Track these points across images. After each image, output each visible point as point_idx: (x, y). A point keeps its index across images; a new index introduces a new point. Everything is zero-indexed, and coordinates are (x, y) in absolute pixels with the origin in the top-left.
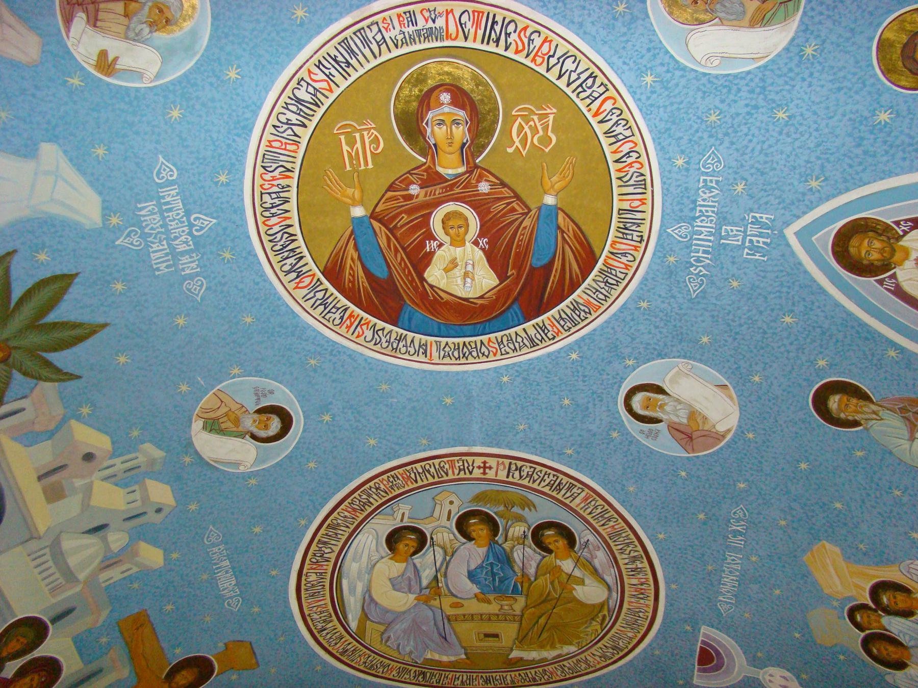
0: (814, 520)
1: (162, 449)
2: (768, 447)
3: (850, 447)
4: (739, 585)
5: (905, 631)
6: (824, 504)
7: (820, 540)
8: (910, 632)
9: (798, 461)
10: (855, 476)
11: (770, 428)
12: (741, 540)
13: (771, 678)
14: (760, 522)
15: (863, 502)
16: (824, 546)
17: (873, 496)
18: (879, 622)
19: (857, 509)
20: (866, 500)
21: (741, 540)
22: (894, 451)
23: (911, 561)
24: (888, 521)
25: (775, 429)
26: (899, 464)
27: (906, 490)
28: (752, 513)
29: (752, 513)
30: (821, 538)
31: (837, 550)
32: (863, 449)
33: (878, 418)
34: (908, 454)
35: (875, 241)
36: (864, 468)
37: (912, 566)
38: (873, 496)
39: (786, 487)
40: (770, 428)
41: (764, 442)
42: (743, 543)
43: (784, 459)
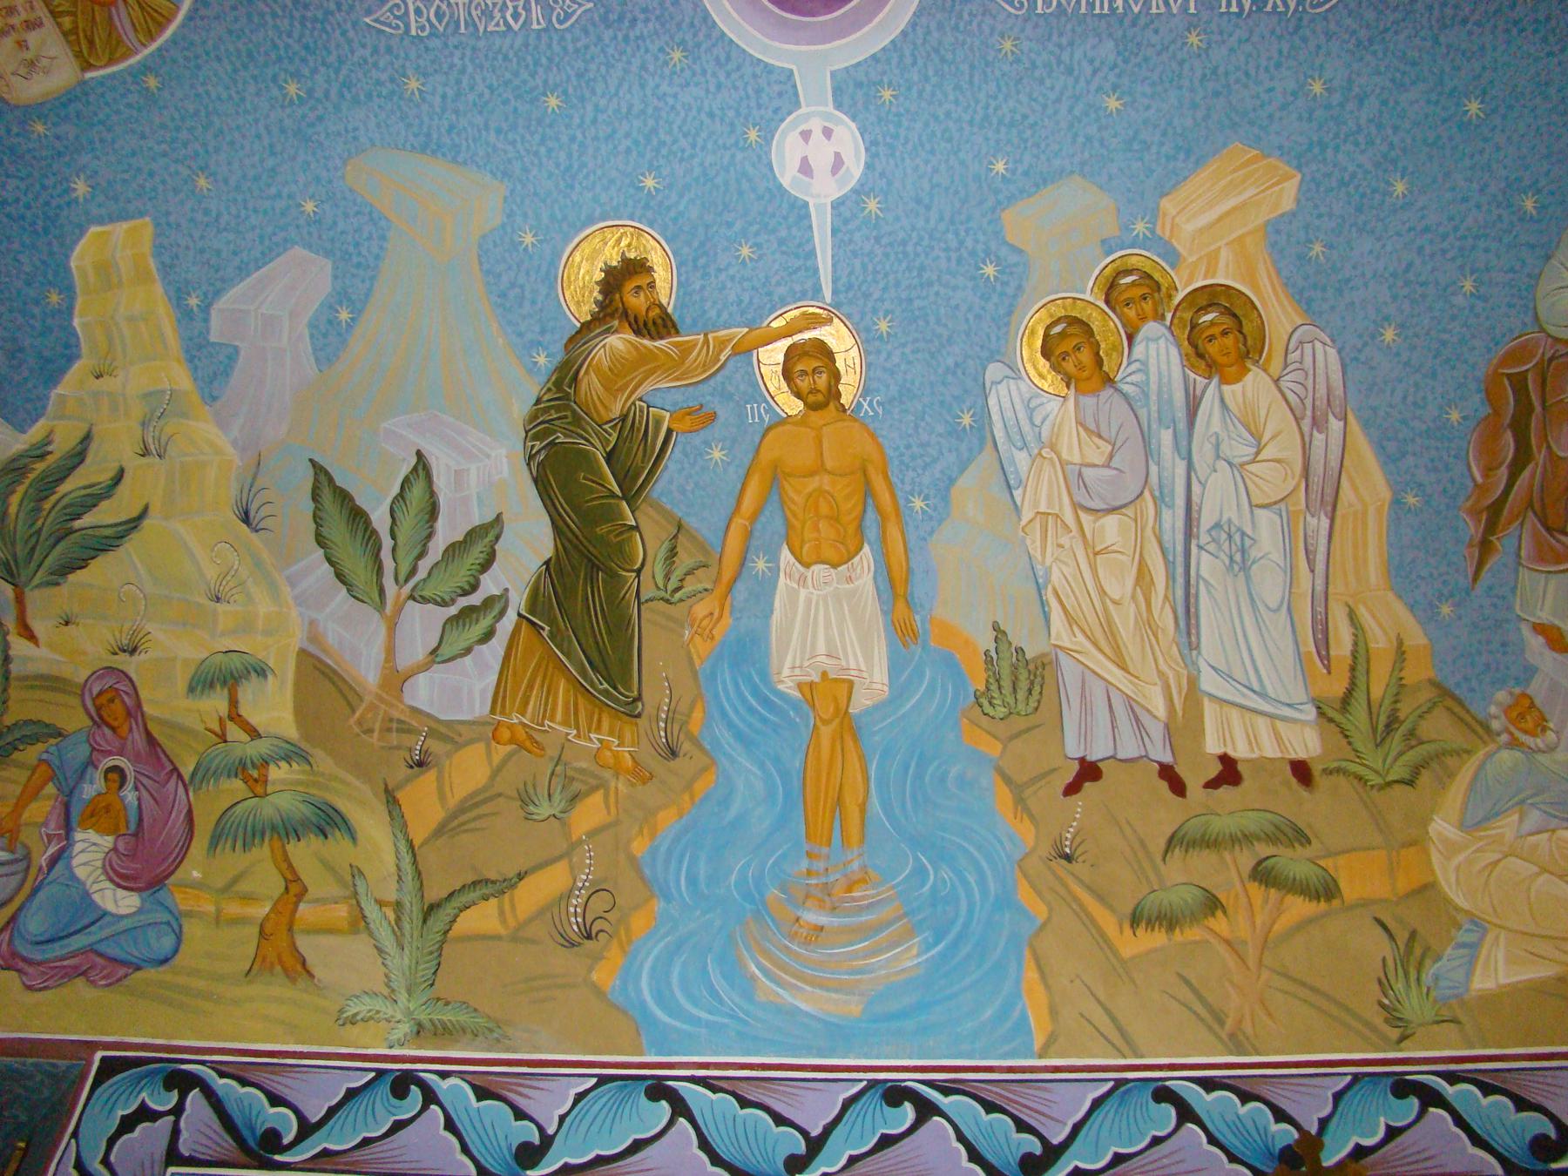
0: (1349, 147)
1: (798, 395)
2: (1507, 31)
3: (1540, 185)
4: (1101, 16)
5: (1153, 369)
6: (1394, 162)
7: (1299, 168)
8: (1153, 378)
9: (1484, 93)
10: (1478, 206)
11: (1553, 31)
12: (760, 417)
13: (817, 134)
14: (1304, 40)
15: (1426, 230)
16: (1287, 178)
17: (1445, 245)
18: (1143, 319)
19: (1404, 223)
20: (1428, 236)
21: (760, 417)
22: (1554, 261)
23: (1328, 341)
24: (1400, 283)
25: (1551, 39)
26: (1529, 275)
27: (1479, 298)
28: (1325, 19)
29: (1325, 19)
30: (1305, 170)
31: (1288, 204)
32: (1541, 208)
33: (323, 478)
34: (1555, 286)
35: (824, 376)
36: (1500, 216)
37: (1318, 345)
38: (1445, 245)
39: (1413, 83)
40: (1553, 31)
41: (1516, 23)
42: (1234, 9)
43: (1484, 68)
